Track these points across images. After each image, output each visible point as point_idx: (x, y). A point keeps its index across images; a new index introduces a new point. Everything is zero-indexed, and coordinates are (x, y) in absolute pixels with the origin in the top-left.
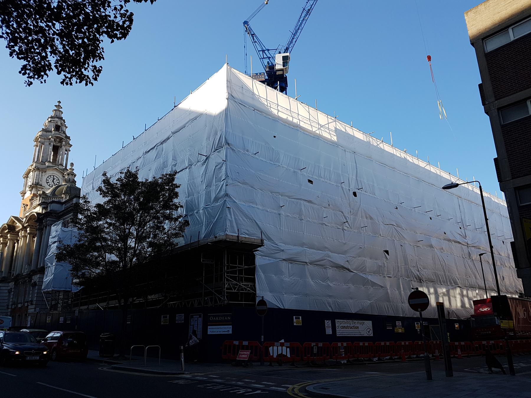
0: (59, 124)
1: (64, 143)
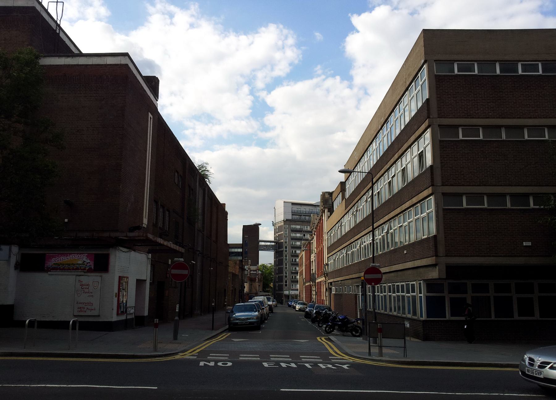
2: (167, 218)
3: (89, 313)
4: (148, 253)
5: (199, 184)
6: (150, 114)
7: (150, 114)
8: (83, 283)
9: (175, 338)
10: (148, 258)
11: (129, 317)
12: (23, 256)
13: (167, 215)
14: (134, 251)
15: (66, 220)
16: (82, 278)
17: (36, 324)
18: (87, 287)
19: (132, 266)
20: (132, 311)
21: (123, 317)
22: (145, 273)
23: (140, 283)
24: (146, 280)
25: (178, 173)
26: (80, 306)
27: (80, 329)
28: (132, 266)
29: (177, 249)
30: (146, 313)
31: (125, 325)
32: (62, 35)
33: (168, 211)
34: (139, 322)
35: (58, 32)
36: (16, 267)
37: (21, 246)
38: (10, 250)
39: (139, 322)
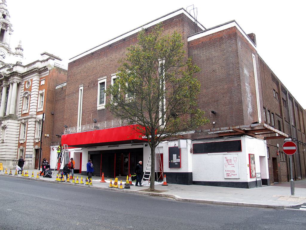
0: (5, 13)
1: (9, 28)
2: (272, 118)
3: (233, 177)
4: (264, 139)
5: (289, 98)
6: (253, 54)
7: (253, 54)
8: (228, 159)
9: (293, 193)
10: (265, 143)
11: (258, 180)
12: (194, 145)
13: (272, 116)
14: (256, 138)
15: (214, 123)
16: (226, 156)
17: (5, 29)
18: (230, 161)
19: (255, 147)
20: (259, 176)
21: (254, 180)
22: (264, 152)
23: (261, 158)
24: (265, 157)
25: (275, 91)
26: (228, 172)
27: (168, 181)
28: (255, 147)
29: (284, 135)
30: (268, 178)
31: (256, 184)
32: (198, 25)
33: (272, 113)
34: (264, 182)
35: (196, 23)
36: (191, 152)
37: (193, 140)
38: (187, 142)
39: (264, 182)
